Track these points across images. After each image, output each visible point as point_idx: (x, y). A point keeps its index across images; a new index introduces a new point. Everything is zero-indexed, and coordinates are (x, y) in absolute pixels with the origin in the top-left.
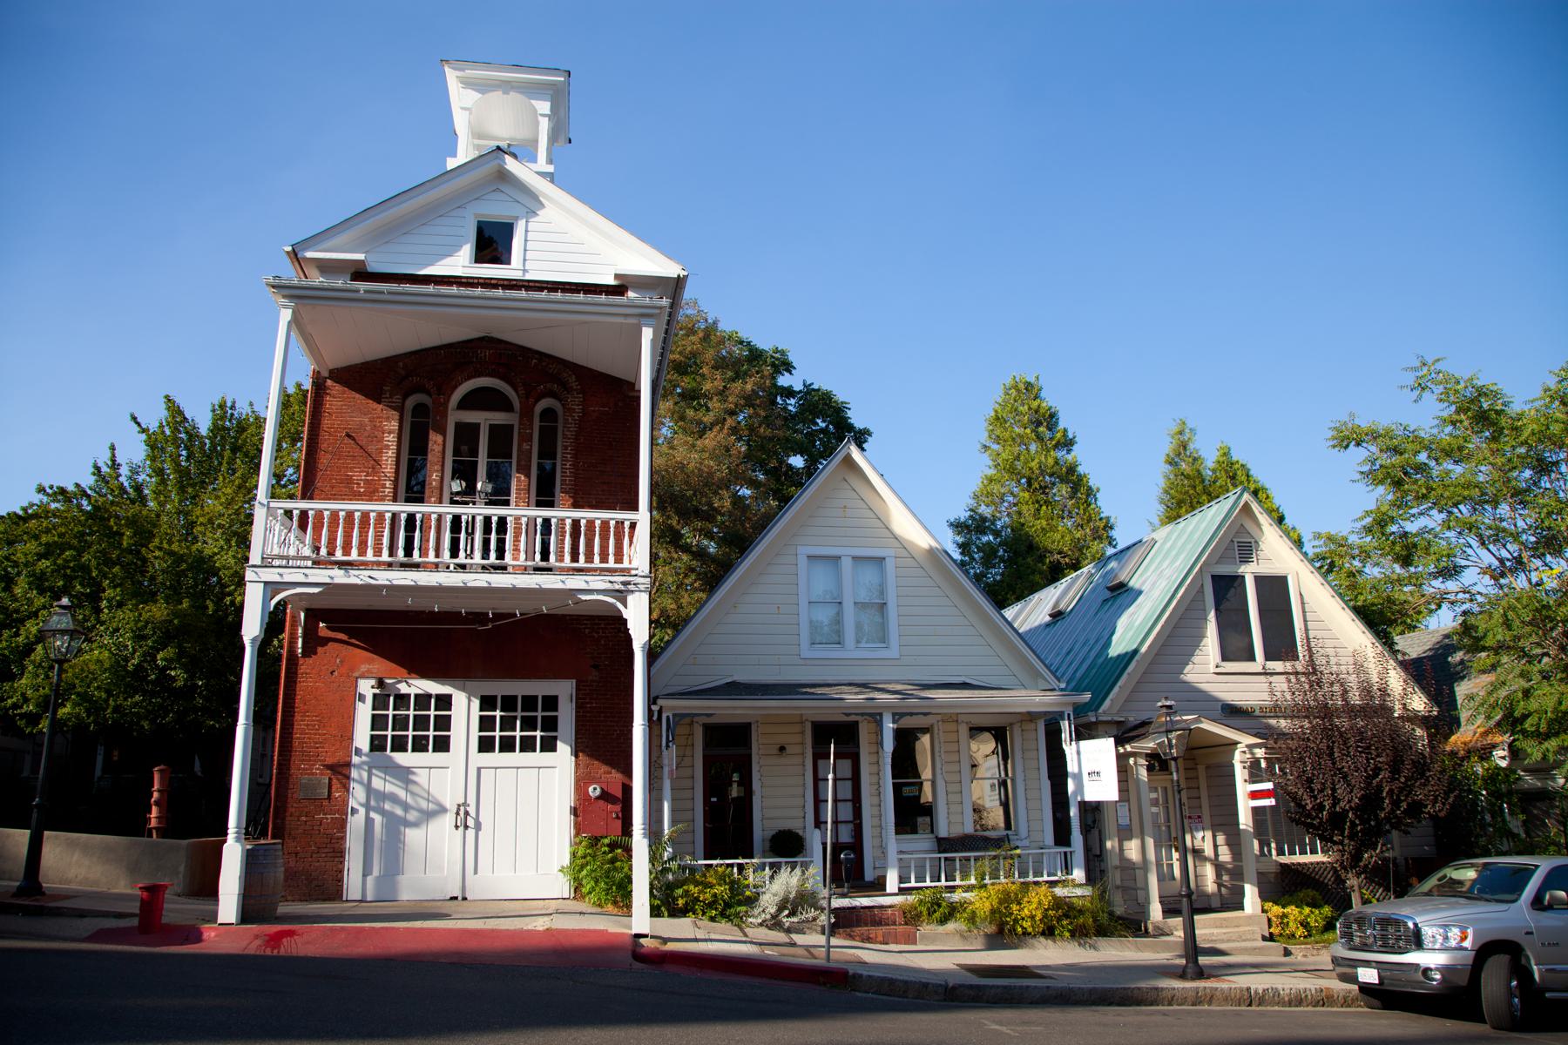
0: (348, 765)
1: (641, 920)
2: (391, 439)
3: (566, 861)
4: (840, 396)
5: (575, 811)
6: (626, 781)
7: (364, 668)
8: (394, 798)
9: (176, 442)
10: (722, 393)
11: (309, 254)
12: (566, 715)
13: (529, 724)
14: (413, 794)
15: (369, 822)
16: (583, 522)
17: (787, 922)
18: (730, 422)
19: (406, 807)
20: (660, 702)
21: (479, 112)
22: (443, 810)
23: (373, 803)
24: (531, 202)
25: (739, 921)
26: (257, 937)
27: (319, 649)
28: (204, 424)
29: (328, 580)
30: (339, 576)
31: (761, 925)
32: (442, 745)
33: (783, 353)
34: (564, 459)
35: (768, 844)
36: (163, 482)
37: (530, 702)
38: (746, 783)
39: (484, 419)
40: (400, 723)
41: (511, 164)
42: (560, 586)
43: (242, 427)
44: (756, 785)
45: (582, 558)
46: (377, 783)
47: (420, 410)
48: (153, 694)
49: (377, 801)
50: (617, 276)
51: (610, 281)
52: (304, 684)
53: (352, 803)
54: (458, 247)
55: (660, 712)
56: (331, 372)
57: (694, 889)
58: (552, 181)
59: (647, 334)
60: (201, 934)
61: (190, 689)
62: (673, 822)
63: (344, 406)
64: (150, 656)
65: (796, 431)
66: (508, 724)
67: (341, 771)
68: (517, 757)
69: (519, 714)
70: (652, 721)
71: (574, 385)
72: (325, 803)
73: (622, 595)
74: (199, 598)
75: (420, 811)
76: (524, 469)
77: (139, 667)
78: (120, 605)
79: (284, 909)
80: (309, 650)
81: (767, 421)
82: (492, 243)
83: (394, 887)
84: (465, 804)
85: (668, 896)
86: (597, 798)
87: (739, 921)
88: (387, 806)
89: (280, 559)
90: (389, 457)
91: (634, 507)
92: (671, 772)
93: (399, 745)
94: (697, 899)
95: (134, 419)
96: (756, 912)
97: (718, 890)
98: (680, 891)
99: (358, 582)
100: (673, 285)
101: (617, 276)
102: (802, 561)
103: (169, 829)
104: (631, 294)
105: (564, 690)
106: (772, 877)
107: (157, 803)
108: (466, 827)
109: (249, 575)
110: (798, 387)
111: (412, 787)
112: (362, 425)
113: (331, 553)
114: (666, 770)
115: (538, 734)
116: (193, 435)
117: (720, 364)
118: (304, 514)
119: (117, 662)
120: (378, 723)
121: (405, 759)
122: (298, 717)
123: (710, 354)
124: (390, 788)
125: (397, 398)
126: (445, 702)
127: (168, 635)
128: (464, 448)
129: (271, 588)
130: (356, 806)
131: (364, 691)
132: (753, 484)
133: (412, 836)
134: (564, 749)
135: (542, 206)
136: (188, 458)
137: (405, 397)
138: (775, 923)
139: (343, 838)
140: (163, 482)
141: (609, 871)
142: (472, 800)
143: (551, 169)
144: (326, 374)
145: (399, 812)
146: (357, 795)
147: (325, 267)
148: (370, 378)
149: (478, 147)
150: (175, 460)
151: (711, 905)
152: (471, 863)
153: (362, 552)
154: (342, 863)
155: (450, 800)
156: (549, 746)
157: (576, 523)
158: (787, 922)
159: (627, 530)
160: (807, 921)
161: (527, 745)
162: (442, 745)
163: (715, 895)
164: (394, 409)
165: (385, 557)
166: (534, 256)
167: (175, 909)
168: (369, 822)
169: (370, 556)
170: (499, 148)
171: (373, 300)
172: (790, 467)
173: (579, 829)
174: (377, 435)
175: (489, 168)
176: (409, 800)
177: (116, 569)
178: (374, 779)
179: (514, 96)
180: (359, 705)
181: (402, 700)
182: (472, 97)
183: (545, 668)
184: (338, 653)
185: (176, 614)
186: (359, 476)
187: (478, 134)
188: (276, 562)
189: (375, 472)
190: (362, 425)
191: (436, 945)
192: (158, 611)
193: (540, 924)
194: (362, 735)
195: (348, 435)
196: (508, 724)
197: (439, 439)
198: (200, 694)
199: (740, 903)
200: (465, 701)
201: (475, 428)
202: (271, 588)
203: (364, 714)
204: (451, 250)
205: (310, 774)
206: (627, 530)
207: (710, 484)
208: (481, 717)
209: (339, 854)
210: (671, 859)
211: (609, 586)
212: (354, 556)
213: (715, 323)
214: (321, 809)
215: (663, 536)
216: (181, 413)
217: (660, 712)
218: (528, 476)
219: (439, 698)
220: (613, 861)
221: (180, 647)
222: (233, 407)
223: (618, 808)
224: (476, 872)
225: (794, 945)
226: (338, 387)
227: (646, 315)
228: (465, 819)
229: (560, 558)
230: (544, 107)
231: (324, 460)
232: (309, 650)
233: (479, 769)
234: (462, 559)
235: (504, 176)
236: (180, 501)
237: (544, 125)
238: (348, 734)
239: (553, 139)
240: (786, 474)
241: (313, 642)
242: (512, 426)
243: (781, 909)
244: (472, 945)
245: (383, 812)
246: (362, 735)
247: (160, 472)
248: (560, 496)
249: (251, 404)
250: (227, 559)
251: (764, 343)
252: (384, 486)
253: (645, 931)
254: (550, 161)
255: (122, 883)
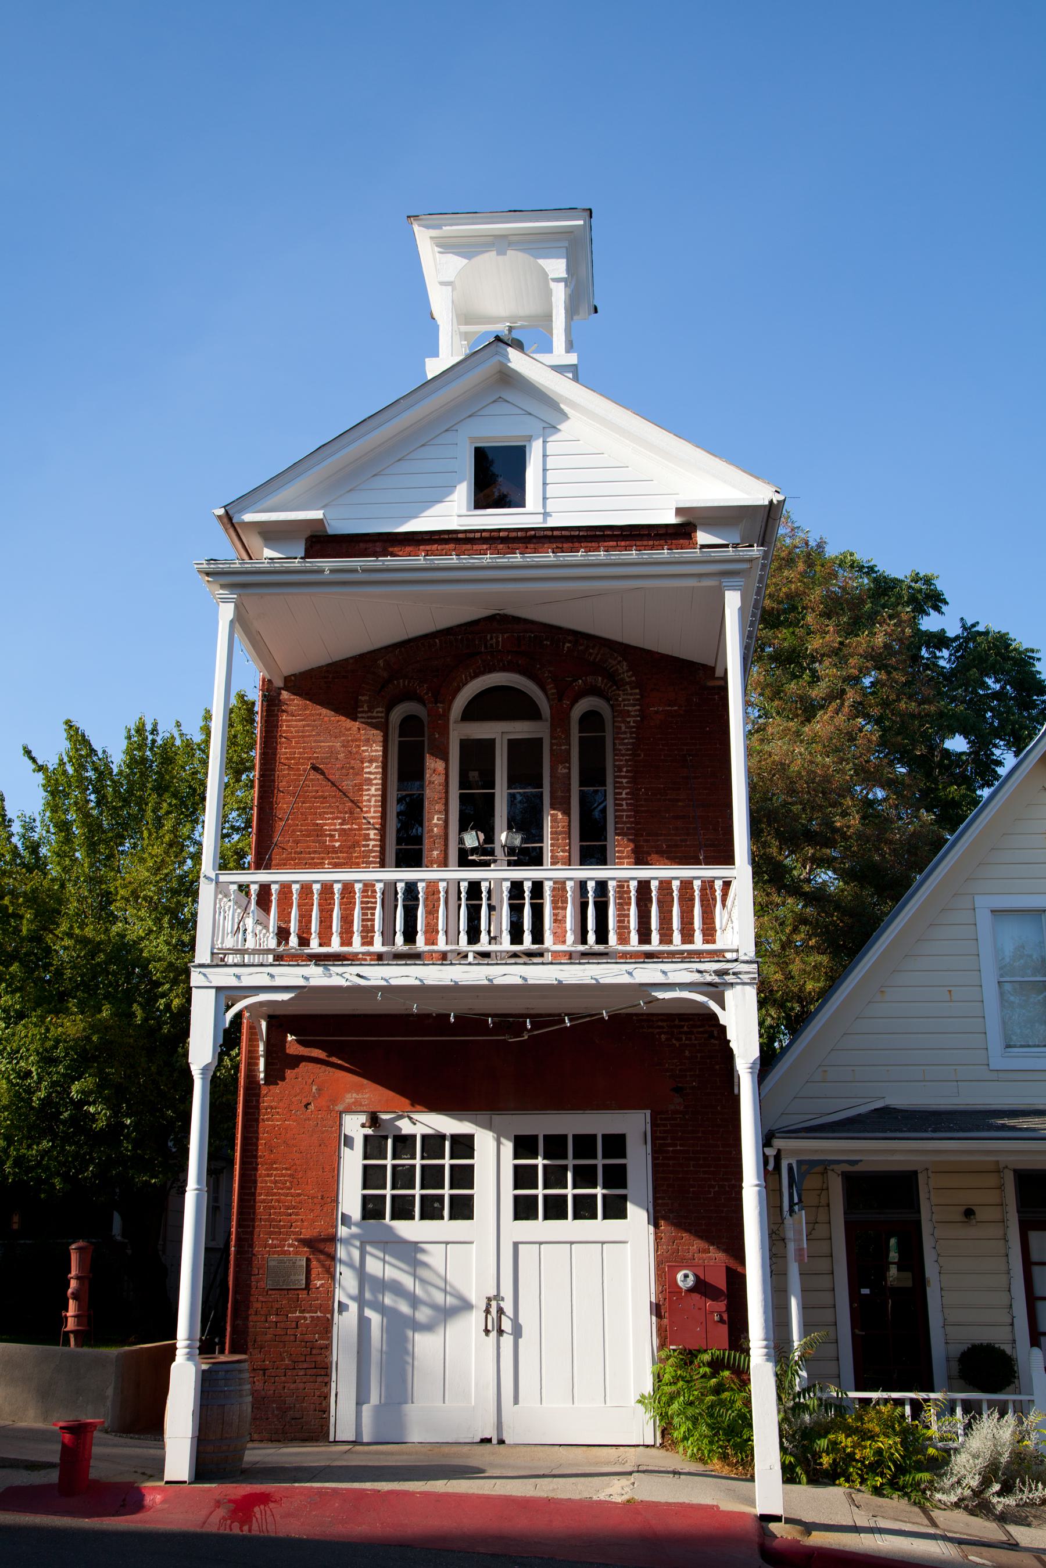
0: (333, 1239)
1: (768, 1492)
2: (373, 770)
3: (648, 1388)
4: (1022, 639)
5: (657, 1310)
6: (733, 1264)
7: (350, 1098)
8: (396, 1288)
9: (82, 783)
10: (838, 653)
11: (249, 517)
12: (639, 1163)
13: (586, 1177)
14: (423, 1281)
15: (363, 1323)
16: (654, 885)
17: (1000, 1503)
18: (851, 696)
19: (414, 1301)
20: (778, 1143)
21: (465, 287)
22: (466, 1306)
23: (368, 1295)
24: (548, 412)
25: (919, 1497)
26: (218, 1504)
27: (289, 1073)
28: (115, 751)
29: (302, 982)
30: (316, 976)
31: (957, 1505)
32: (463, 1209)
33: (928, 581)
34: (617, 785)
35: (955, 1367)
36: (68, 840)
37: (585, 1144)
38: (913, 1259)
39: (499, 732)
40: (404, 1177)
41: (516, 360)
42: (626, 979)
43: (167, 755)
44: (931, 1270)
45: (655, 937)
46: (374, 1266)
47: (410, 725)
48: (67, 1139)
49: (373, 1292)
50: (679, 511)
51: (670, 518)
52: (270, 1122)
53: (339, 1296)
54: (451, 488)
55: (778, 1158)
56: (287, 679)
57: (846, 1442)
58: (576, 379)
59: (733, 601)
60: (142, 1497)
61: (115, 1129)
62: (807, 1327)
63: (310, 729)
64: (61, 1087)
65: (953, 699)
66: (555, 1177)
67: (322, 1248)
68: (569, 1227)
69: (570, 1162)
70: (770, 1171)
71: (627, 676)
72: (303, 1295)
73: (716, 991)
74: (123, 1001)
75: (434, 1307)
76: (562, 803)
77: (46, 1102)
78: (21, 1016)
79: (257, 1454)
80: (274, 1075)
81: (908, 689)
82: (497, 476)
83: (400, 1422)
84: (498, 1297)
85: (806, 1449)
86: (690, 1290)
87: (919, 1497)
88: (388, 1300)
89: (235, 955)
90: (372, 794)
91: (728, 859)
92: (800, 1250)
93: (403, 1210)
94: (851, 1457)
95: (28, 752)
96: (947, 1482)
97: (884, 1443)
98: (823, 1443)
99: (343, 983)
100: (761, 517)
101: (679, 511)
102: (984, 919)
103: (93, 1333)
104: (703, 537)
105: (634, 1125)
106: (968, 1427)
107: (76, 1296)
108: (501, 1332)
109: (196, 978)
110: (953, 630)
111: (422, 1272)
112: (332, 751)
113: (304, 942)
114: (791, 1247)
115: (599, 1191)
116: (103, 772)
117: (832, 607)
118: (265, 890)
119: (17, 1095)
120: (371, 1176)
121: (411, 1229)
122: (262, 1171)
123: (817, 594)
124: (391, 1273)
125: (379, 711)
126: (464, 1145)
127: (84, 1057)
128: (474, 775)
129: (227, 996)
130: (344, 1300)
131: (350, 1127)
132: (889, 784)
133: (424, 1344)
134: (637, 1216)
135: (565, 416)
136: (99, 803)
137: (389, 710)
138: (977, 1505)
139: (328, 1347)
140: (68, 840)
141: (712, 1406)
142: (507, 1292)
143: (572, 359)
144: (279, 683)
145: (404, 1308)
146: (347, 1283)
147: (271, 533)
148: (340, 685)
149: (465, 336)
150: (81, 807)
151: (875, 1467)
152: (509, 1387)
153: (346, 941)
154: (327, 1384)
155: (476, 1292)
156: (616, 1210)
157: (644, 886)
158: (1000, 1503)
159: (718, 894)
160: (1032, 1504)
161: (585, 1209)
162: (463, 1209)
163: (879, 1452)
164: (375, 726)
165: (378, 946)
166: (562, 490)
167: (109, 1458)
168: (363, 1323)
169: (357, 945)
170: (498, 339)
171: (342, 582)
172: (947, 753)
173: (664, 1338)
174: (353, 767)
175: (486, 368)
176: (419, 1292)
177: (14, 968)
178: (369, 1260)
179: (514, 256)
180: (346, 1152)
181: (404, 1143)
182: (453, 264)
183: (606, 1096)
184: (315, 1078)
185: (94, 1028)
186: (332, 824)
187: (465, 317)
188: (230, 959)
189: (353, 819)
190: (332, 751)
191: (471, 1523)
192: (71, 1026)
193: (616, 1491)
194: (351, 1197)
195: (315, 768)
196: (555, 1177)
197: (440, 765)
198: (127, 1137)
199: (920, 1467)
200: (493, 1144)
201: (487, 747)
202: (227, 996)
203: (352, 1163)
204: (439, 494)
205: (280, 1253)
206: (718, 894)
207: (825, 793)
208: (516, 1168)
209: (323, 1371)
210: (805, 1391)
211: (696, 977)
212: (335, 946)
213: (820, 546)
214: (296, 1304)
215: (768, 874)
216: (85, 741)
217: (778, 1158)
218: (567, 812)
219: (456, 1139)
220: (718, 1390)
221: (100, 1073)
222: (154, 731)
223: (722, 1305)
224: (516, 1401)
225: (1013, 1546)
226: (297, 701)
227: (729, 574)
228: (500, 1320)
229: (623, 939)
230: (556, 267)
231: (284, 804)
232: (274, 1075)
233: (516, 1245)
234: (483, 945)
235: (508, 379)
236: (91, 865)
237: (559, 294)
238: (331, 1196)
239: (572, 309)
240: (940, 765)
241: (280, 1063)
242: (540, 740)
243: (986, 1483)
244: (520, 1524)
245: (382, 1309)
246: (351, 1197)
247: (64, 827)
248: (617, 844)
249: (178, 725)
250: (158, 946)
251: (896, 567)
252: (367, 838)
253: (778, 1511)
254: (570, 347)
255: (31, 1413)
